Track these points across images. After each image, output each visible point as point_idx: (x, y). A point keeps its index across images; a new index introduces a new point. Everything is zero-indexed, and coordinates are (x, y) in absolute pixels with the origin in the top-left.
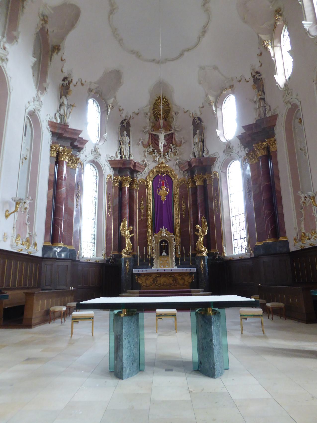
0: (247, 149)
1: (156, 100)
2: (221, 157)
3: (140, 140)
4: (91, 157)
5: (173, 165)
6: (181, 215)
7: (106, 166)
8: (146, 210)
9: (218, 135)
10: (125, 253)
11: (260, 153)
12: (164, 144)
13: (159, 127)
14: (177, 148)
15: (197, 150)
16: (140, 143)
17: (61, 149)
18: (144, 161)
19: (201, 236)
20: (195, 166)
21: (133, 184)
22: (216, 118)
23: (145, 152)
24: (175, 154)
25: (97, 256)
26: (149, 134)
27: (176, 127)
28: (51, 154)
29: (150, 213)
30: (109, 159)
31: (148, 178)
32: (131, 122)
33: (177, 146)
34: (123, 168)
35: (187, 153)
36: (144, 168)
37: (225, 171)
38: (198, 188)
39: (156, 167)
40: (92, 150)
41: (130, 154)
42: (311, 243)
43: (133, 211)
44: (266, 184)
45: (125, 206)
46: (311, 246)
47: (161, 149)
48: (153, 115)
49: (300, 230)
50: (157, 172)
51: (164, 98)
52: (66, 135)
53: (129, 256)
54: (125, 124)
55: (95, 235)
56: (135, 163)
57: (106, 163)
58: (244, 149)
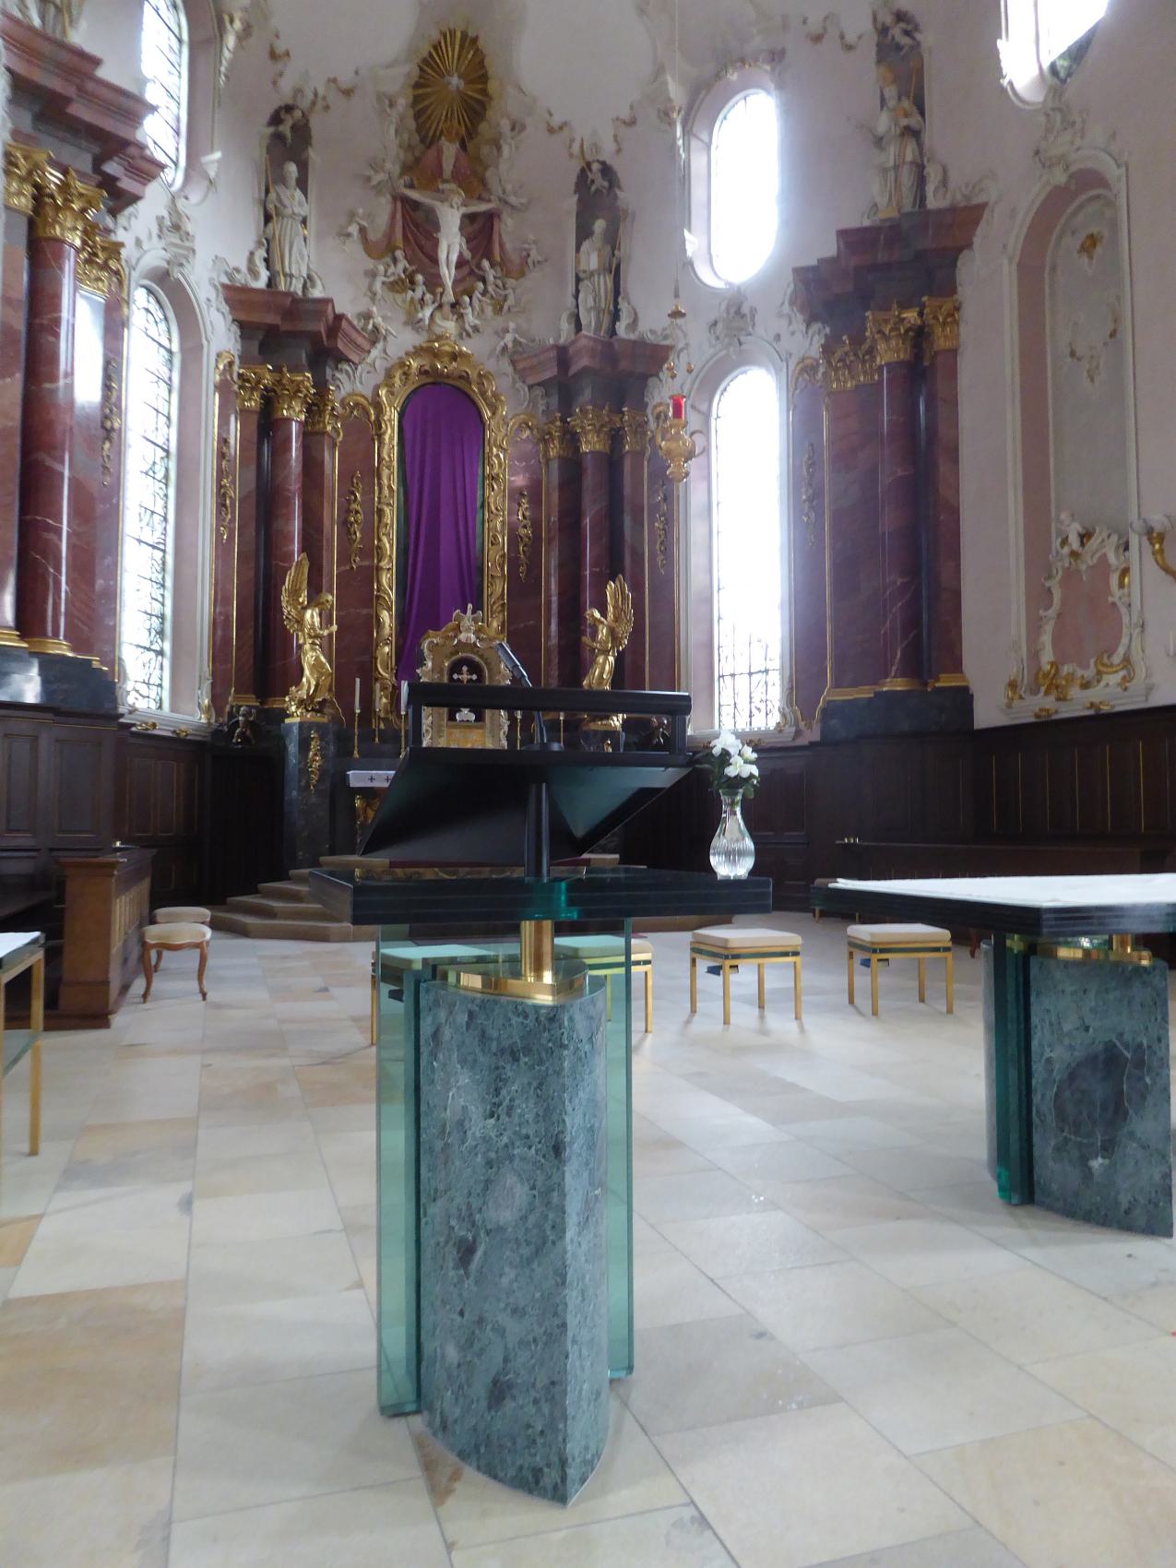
0: (816, 326)
1: (437, 47)
2: (694, 346)
3: (352, 216)
4: (155, 255)
5: (490, 357)
6: (513, 562)
7: (213, 312)
8: (371, 530)
9: (689, 253)
10: (301, 703)
11: (889, 352)
12: (461, 255)
13: (437, 173)
14: (511, 282)
15: (590, 303)
16: (354, 229)
17: (53, 177)
18: (367, 316)
19: (606, 653)
20: (585, 370)
21: (321, 412)
22: (685, 180)
23: (373, 275)
24: (498, 309)
25: (173, 709)
26: (395, 198)
27: (509, 187)
28: (8, 193)
29: (389, 545)
30: (225, 280)
31: (383, 392)
32: (316, 124)
33: (508, 274)
34: (284, 335)
35: (547, 312)
36: (366, 345)
37: (704, 407)
38: (589, 464)
39: (417, 352)
40: (160, 220)
41: (309, 277)
42: (1096, 700)
43: (320, 530)
44: (900, 473)
45: (288, 503)
46: (1091, 712)
47: (448, 274)
48: (411, 113)
49: (1034, 655)
50: (422, 372)
51: (469, 42)
52: (79, 110)
53: (319, 718)
54: (285, 128)
55: (162, 617)
56: (339, 318)
57: (213, 296)
58: (803, 327)
